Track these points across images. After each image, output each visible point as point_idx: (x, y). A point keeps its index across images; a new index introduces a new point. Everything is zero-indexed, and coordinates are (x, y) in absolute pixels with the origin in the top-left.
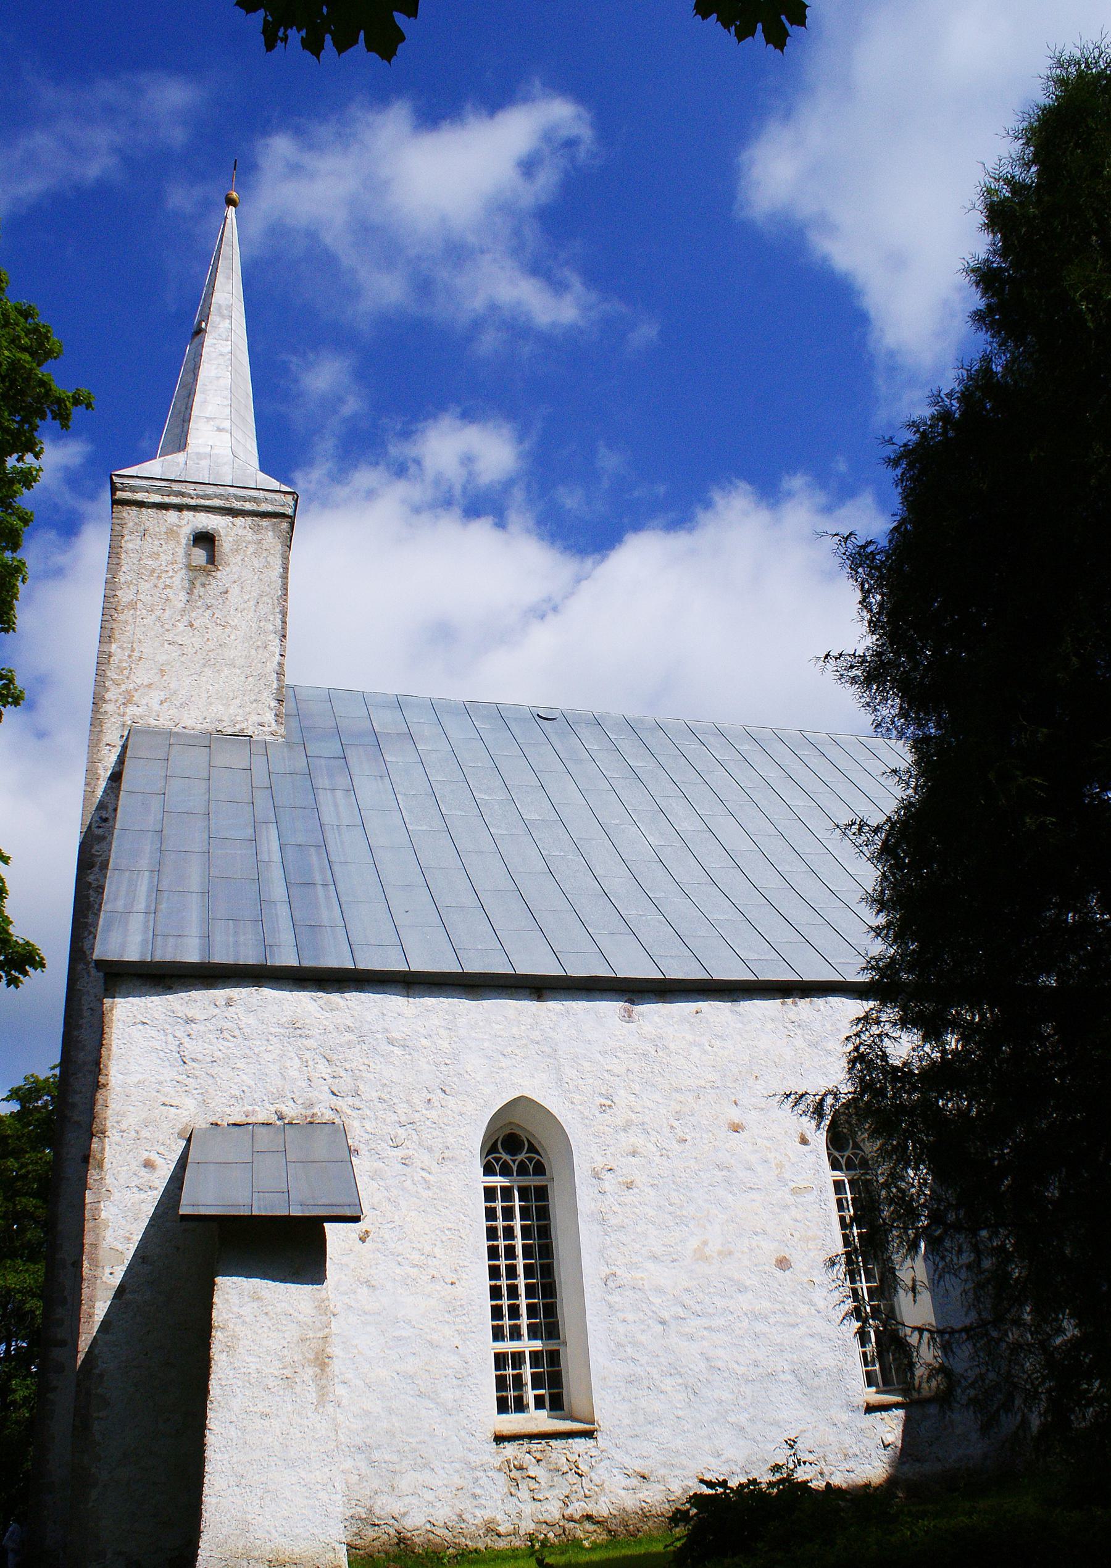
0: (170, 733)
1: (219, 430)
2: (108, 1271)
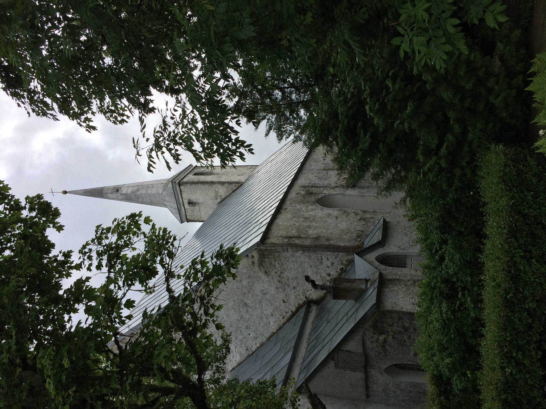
0: (397, 267)
2: (418, 361)
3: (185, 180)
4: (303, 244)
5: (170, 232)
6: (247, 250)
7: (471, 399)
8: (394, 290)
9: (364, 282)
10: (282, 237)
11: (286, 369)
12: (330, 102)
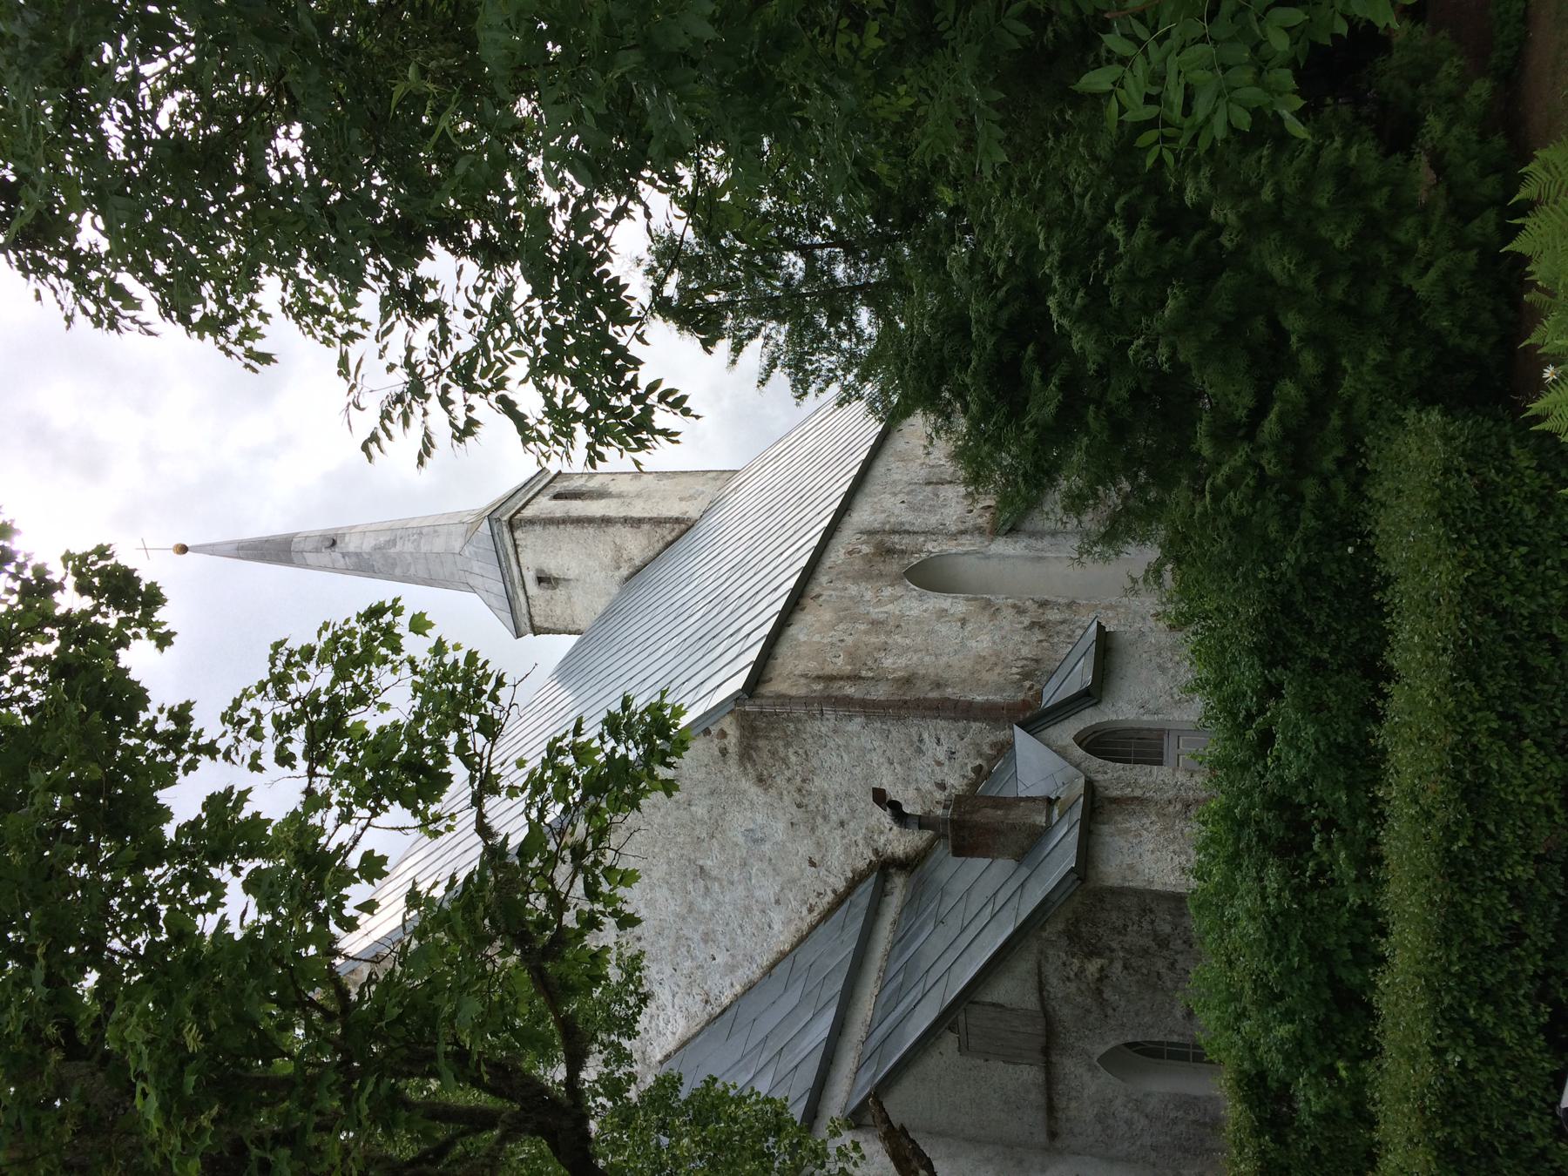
1: (436, 884)
3: (528, 512)
4: (868, 697)
5: (486, 662)
6: (705, 714)
7: (1350, 1143)
8: (1127, 831)
9: (1042, 806)
10: (805, 676)
11: (819, 1054)
12: (944, 288)
